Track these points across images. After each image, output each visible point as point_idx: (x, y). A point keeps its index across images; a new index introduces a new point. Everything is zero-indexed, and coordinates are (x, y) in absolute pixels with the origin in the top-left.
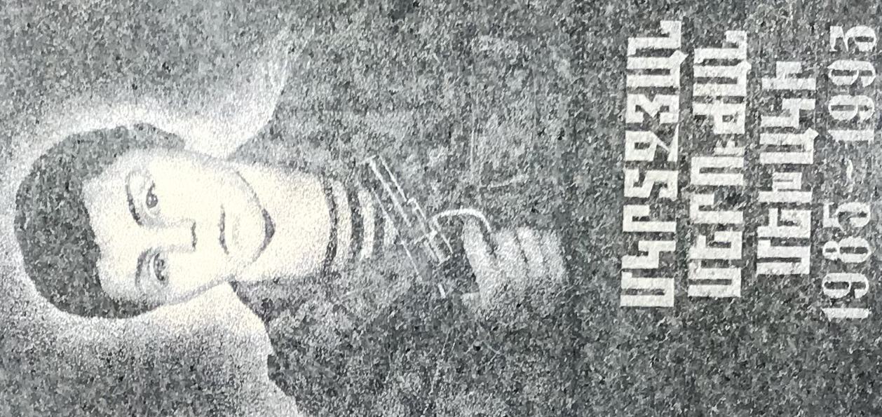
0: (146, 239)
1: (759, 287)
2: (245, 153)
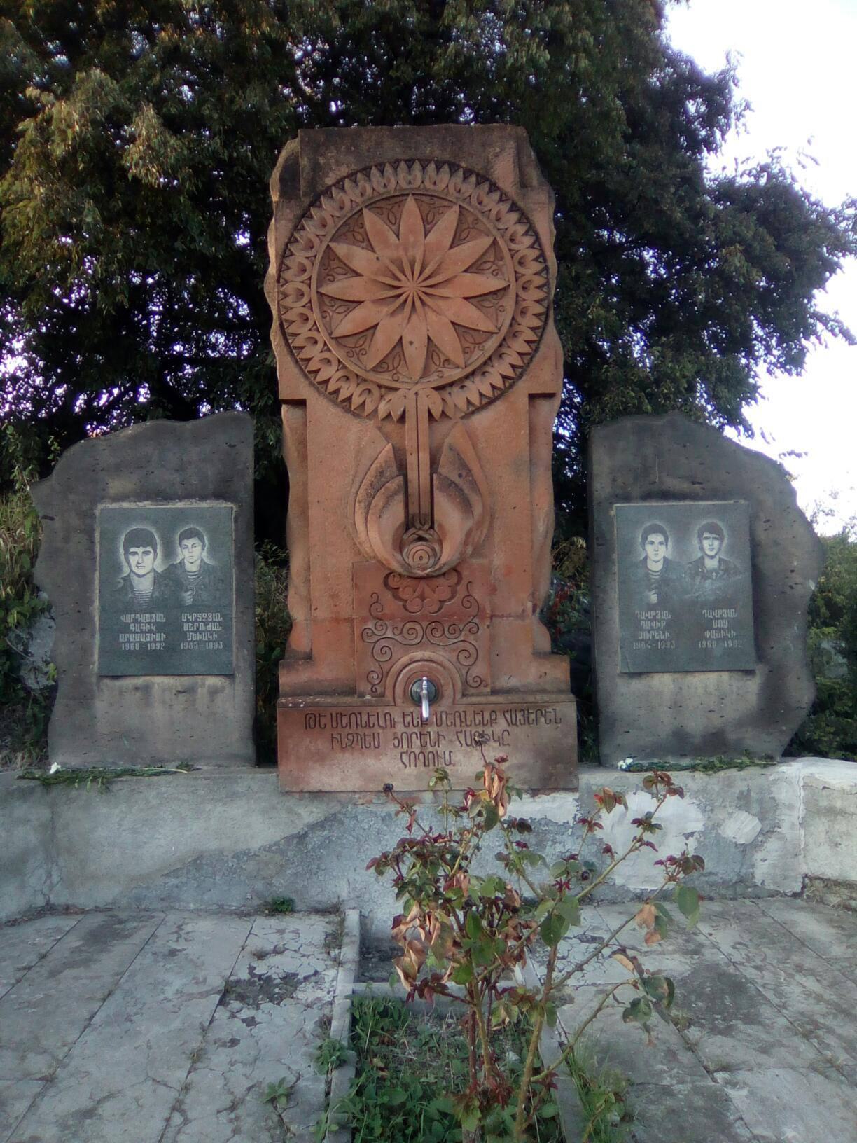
0: (190, 546)
1: (185, 633)
2: (202, 560)
